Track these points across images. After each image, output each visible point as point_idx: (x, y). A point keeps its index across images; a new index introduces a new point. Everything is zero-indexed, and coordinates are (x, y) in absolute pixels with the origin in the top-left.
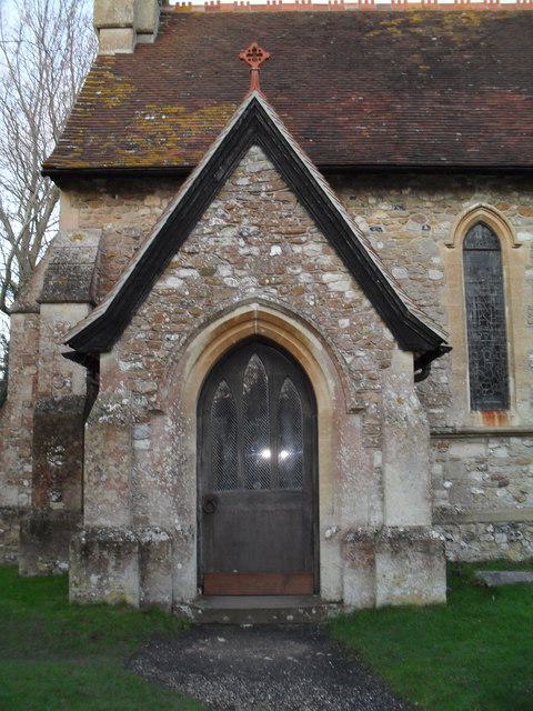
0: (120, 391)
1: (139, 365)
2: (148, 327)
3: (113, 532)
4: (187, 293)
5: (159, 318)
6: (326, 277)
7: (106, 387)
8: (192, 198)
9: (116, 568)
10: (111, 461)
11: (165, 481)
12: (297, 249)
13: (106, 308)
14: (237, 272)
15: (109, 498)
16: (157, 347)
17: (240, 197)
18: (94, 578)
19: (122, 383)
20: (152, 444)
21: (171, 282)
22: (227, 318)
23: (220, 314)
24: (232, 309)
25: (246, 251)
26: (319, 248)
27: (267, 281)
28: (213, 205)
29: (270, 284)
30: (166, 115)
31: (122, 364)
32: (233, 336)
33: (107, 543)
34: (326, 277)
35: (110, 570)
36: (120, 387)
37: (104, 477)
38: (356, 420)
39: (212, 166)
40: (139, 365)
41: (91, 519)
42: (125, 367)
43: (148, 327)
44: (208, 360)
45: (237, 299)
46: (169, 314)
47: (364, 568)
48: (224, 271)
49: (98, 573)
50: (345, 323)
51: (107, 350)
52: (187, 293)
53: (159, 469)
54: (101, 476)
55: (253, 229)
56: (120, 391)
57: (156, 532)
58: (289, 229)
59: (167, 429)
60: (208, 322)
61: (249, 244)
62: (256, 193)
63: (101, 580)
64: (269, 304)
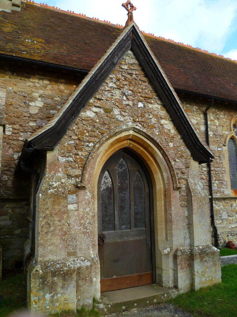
0: (60, 174)
1: (71, 159)
2: (76, 138)
3: (59, 263)
4: (98, 121)
5: (82, 133)
6: (163, 121)
7: (50, 172)
8: (102, 69)
9: (63, 287)
10: (57, 219)
11: (86, 228)
12: (150, 106)
13: (55, 123)
14: (122, 113)
15: (55, 241)
16: (81, 150)
17: (123, 74)
18: (48, 296)
19: (60, 169)
20: (78, 207)
21: (89, 113)
22: (118, 137)
23: (116, 134)
24: (121, 132)
25: (127, 103)
26: (159, 107)
27: (137, 120)
28: (110, 76)
29: (138, 122)
30: (37, 41)
31: (60, 158)
32: (118, 146)
33: (56, 272)
34: (163, 121)
35: (59, 289)
36: (59, 172)
37: (52, 228)
38: (177, 193)
39: (113, 54)
40: (71, 159)
41: (43, 256)
42: (62, 160)
43: (76, 138)
44: (105, 159)
45: (125, 127)
46: (88, 131)
47: (187, 268)
48: (116, 112)
49: (51, 293)
50: (171, 145)
51: (52, 149)
52: (98, 121)
53: (83, 221)
54: (50, 227)
55: (130, 92)
56: (60, 174)
57: (82, 260)
58: (146, 96)
59: (87, 197)
60: (111, 137)
61: (128, 99)
62: (131, 74)
63: (53, 297)
64: (139, 132)
